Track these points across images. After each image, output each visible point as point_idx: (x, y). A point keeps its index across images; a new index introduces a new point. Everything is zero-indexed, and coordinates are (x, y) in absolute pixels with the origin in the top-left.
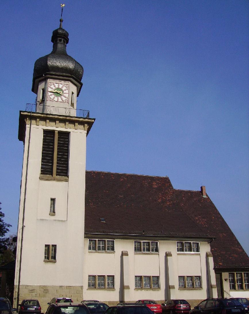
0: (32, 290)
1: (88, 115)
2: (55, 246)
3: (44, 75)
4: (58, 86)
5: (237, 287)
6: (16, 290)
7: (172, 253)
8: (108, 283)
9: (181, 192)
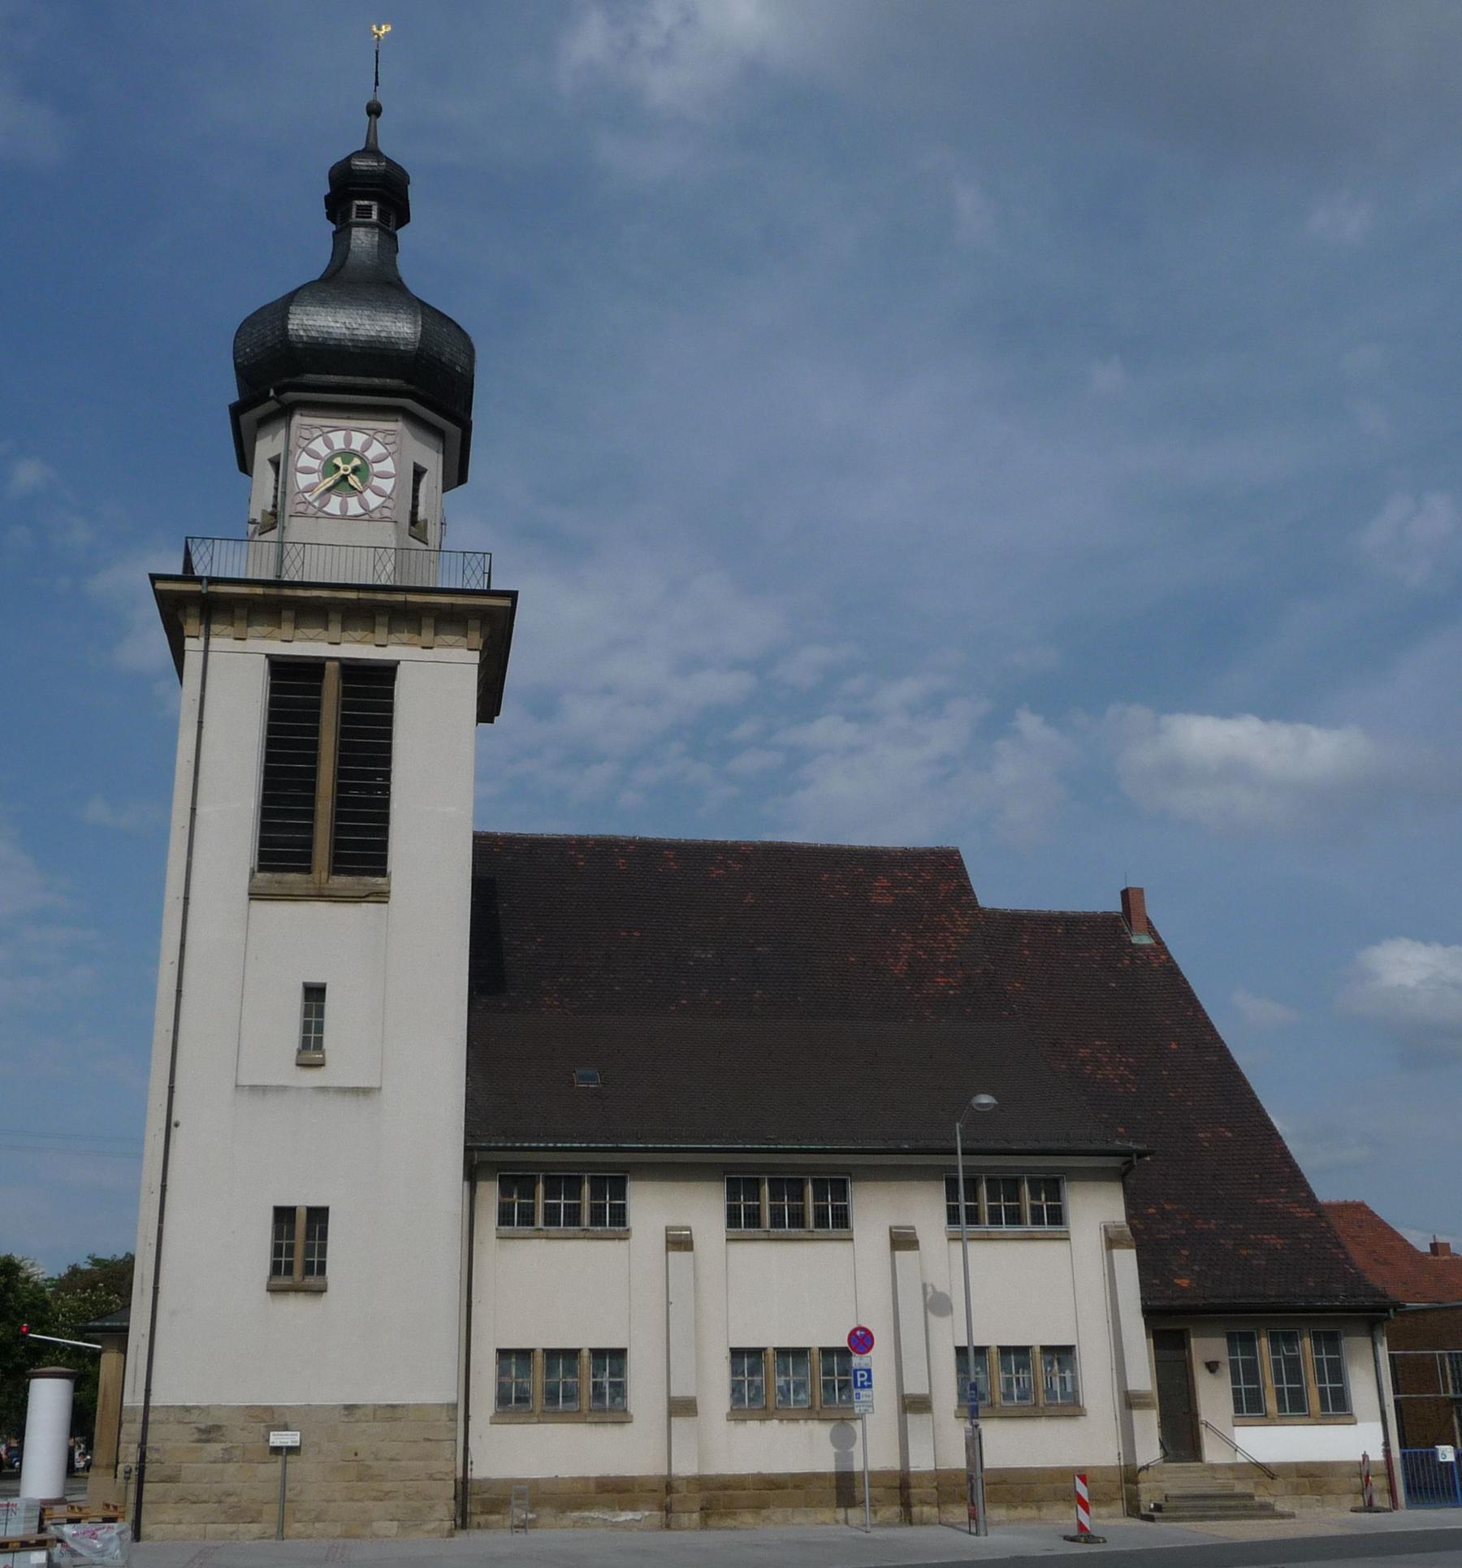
2: (318, 1216)
3: (272, 393)
4: (348, 440)
5: (1271, 1404)
6: (132, 1430)
7: (920, 1236)
8: (597, 1386)
9: (1016, 921)
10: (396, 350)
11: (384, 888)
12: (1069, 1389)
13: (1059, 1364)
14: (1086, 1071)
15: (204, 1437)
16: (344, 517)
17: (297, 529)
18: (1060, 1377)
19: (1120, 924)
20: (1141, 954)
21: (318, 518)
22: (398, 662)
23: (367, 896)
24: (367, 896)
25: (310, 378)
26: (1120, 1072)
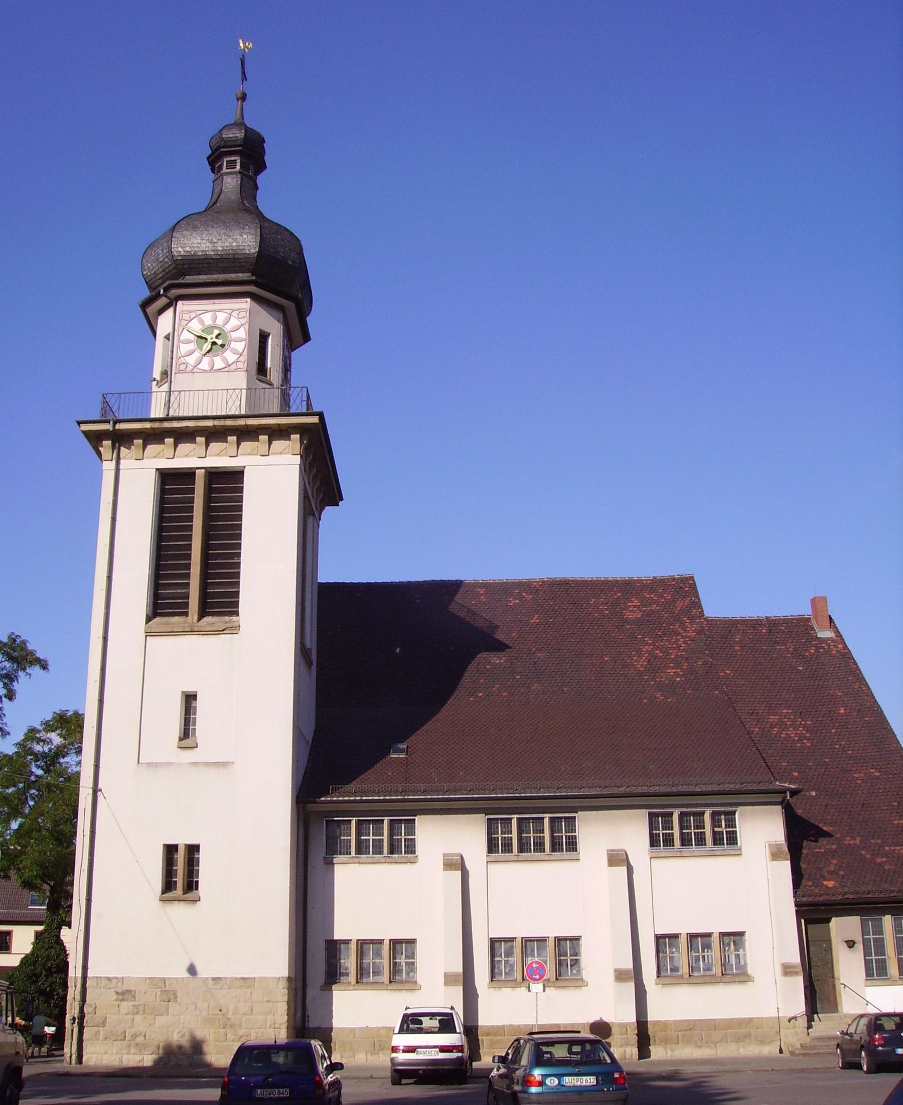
0: (123, 993)
1: (309, 406)
3: (162, 292)
6: (73, 993)
9: (731, 626)
11: (235, 624)
12: (742, 963)
14: (774, 732)
15: (120, 997)
16: (212, 370)
17: (179, 381)
19: (810, 624)
20: (823, 645)
22: (245, 467)
23: (223, 630)
24: (223, 630)
25: (189, 279)
26: (799, 732)
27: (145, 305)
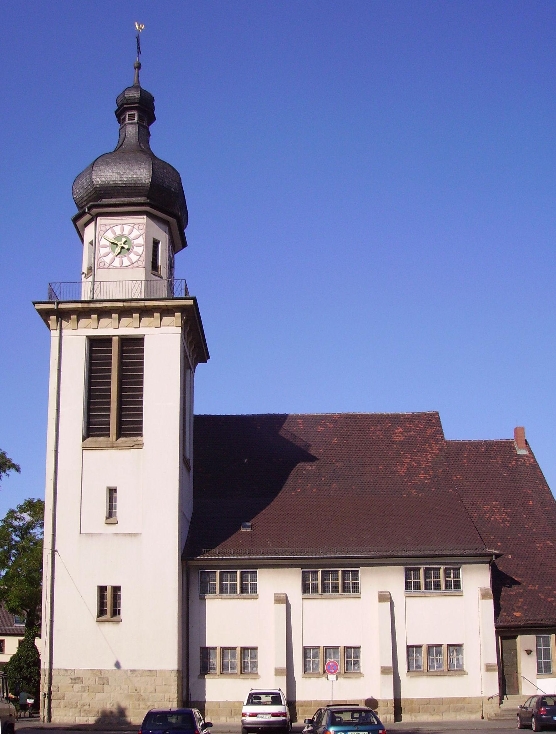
0: (75, 679)
1: (187, 293)
3: (86, 211)
4: (114, 232)
6: (44, 679)
9: (462, 446)
10: (142, 183)
12: (461, 663)
13: (456, 652)
14: (486, 517)
16: (121, 267)
17: (100, 274)
18: (457, 658)
19: (513, 445)
20: (521, 459)
21: (109, 269)
22: (145, 335)
23: (133, 446)
24: (133, 446)
25: (105, 201)
27: (75, 220)
